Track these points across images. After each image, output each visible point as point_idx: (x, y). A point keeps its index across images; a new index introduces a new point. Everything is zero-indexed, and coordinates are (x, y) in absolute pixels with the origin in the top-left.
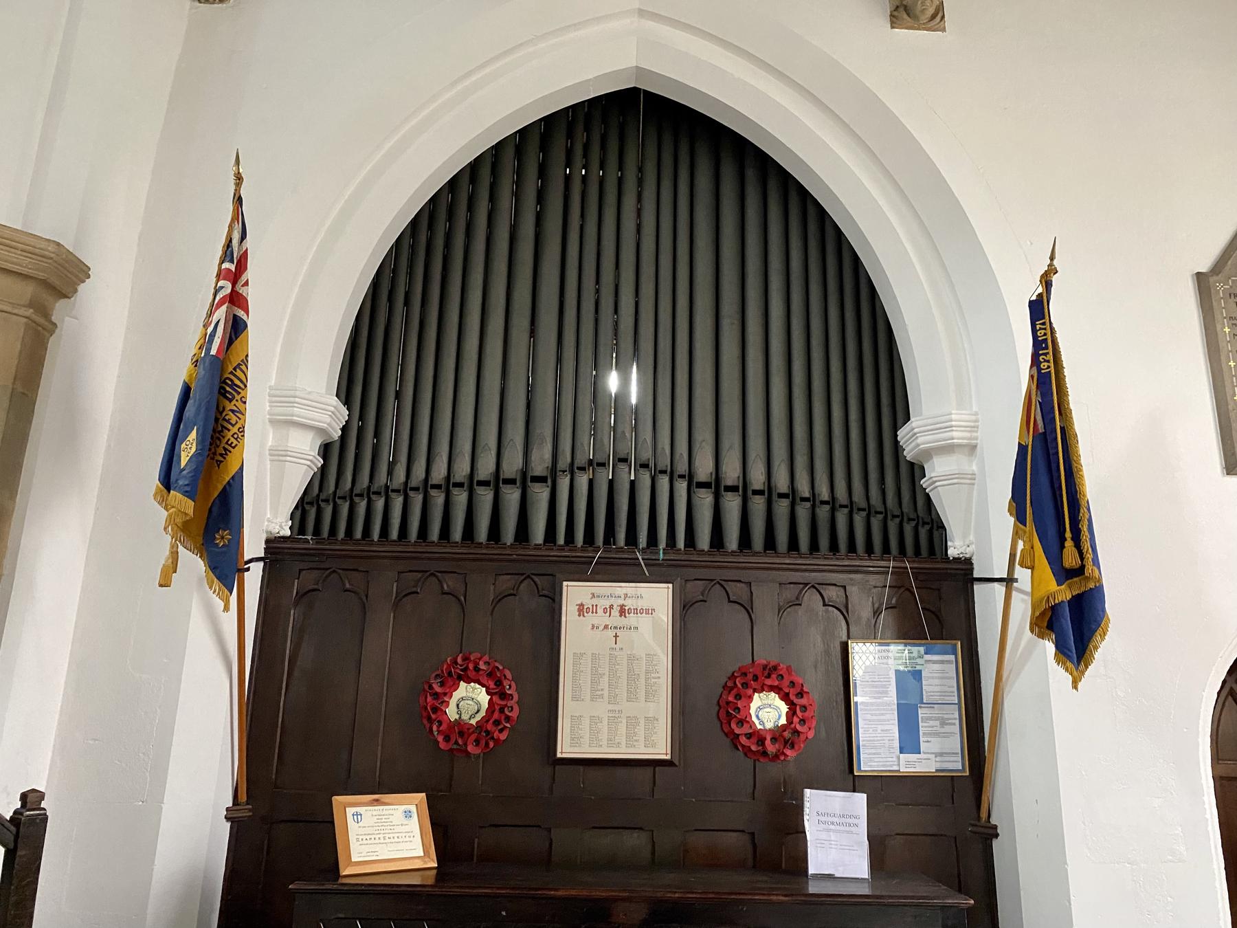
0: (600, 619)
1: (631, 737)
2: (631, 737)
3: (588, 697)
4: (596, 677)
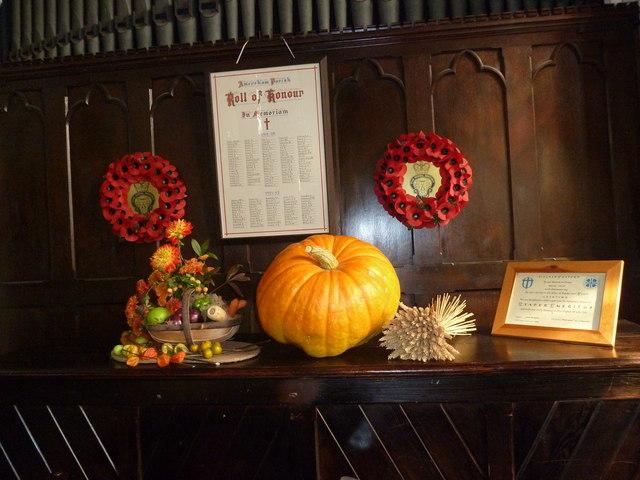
0: (249, 106)
1: (289, 218)
2: (289, 218)
3: (246, 182)
4: (251, 162)
